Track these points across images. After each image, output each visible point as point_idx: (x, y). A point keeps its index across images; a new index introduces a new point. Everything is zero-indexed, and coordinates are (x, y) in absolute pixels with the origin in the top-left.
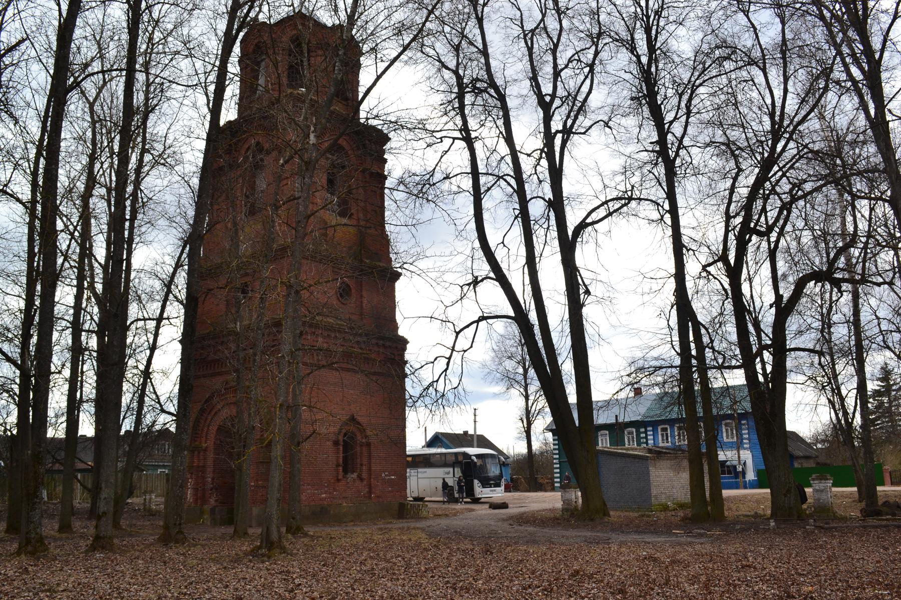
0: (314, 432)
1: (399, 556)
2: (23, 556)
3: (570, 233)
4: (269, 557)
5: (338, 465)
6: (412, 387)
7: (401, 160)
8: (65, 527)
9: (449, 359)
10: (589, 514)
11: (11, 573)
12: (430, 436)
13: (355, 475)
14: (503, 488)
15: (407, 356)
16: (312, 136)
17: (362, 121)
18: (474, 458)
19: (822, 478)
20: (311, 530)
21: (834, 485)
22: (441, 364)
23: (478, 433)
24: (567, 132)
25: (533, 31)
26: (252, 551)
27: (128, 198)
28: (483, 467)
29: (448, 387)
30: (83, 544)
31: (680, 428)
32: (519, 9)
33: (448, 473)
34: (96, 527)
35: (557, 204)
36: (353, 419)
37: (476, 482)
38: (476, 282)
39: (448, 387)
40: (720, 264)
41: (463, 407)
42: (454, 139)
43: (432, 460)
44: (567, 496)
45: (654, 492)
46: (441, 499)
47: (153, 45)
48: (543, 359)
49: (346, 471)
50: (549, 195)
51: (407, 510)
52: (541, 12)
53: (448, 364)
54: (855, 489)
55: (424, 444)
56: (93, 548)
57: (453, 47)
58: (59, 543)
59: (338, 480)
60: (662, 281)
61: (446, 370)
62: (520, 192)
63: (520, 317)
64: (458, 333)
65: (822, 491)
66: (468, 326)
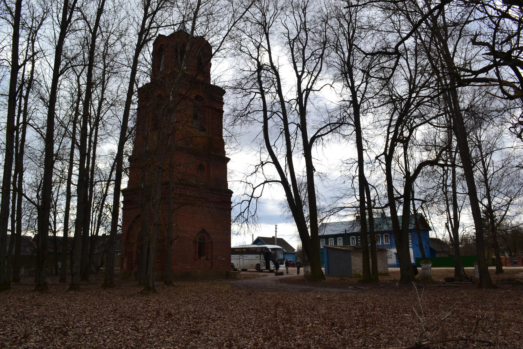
0: (178, 236)
3: (309, 140)
4: (147, 294)
5: (196, 253)
6: (234, 214)
7: (231, 102)
8: (63, 280)
9: (250, 201)
10: (314, 278)
11: (27, 298)
12: (255, 239)
13: (204, 258)
14: (285, 265)
15: (232, 199)
17: (212, 83)
18: (270, 250)
19: (426, 262)
20: (175, 283)
21: (433, 266)
22: (245, 205)
23: (277, 237)
24: (308, 90)
25: (294, 40)
26: (141, 291)
28: (275, 255)
29: (250, 215)
30: (67, 287)
31: (386, 236)
32: (287, 29)
33: (258, 257)
34: (72, 279)
35: (303, 126)
37: (271, 262)
38: (262, 164)
39: (250, 215)
40: (383, 156)
41: (259, 225)
42: (256, 93)
43: (258, 250)
45: (353, 268)
46: (255, 270)
47: (107, 47)
48: (301, 202)
49: (200, 256)
50: (299, 121)
51: (230, 273)
52: (298, 30)
53: (249, 204)
54: (454, 268)
55: (252, 242)
56: (70, 289)
59: (196, 260)
60: (351, 165)
61: (248, 207)
62: (285, 120)
63: (284, 182)
64: (254, 189)
65: (426, 269)
66: (259, 186)
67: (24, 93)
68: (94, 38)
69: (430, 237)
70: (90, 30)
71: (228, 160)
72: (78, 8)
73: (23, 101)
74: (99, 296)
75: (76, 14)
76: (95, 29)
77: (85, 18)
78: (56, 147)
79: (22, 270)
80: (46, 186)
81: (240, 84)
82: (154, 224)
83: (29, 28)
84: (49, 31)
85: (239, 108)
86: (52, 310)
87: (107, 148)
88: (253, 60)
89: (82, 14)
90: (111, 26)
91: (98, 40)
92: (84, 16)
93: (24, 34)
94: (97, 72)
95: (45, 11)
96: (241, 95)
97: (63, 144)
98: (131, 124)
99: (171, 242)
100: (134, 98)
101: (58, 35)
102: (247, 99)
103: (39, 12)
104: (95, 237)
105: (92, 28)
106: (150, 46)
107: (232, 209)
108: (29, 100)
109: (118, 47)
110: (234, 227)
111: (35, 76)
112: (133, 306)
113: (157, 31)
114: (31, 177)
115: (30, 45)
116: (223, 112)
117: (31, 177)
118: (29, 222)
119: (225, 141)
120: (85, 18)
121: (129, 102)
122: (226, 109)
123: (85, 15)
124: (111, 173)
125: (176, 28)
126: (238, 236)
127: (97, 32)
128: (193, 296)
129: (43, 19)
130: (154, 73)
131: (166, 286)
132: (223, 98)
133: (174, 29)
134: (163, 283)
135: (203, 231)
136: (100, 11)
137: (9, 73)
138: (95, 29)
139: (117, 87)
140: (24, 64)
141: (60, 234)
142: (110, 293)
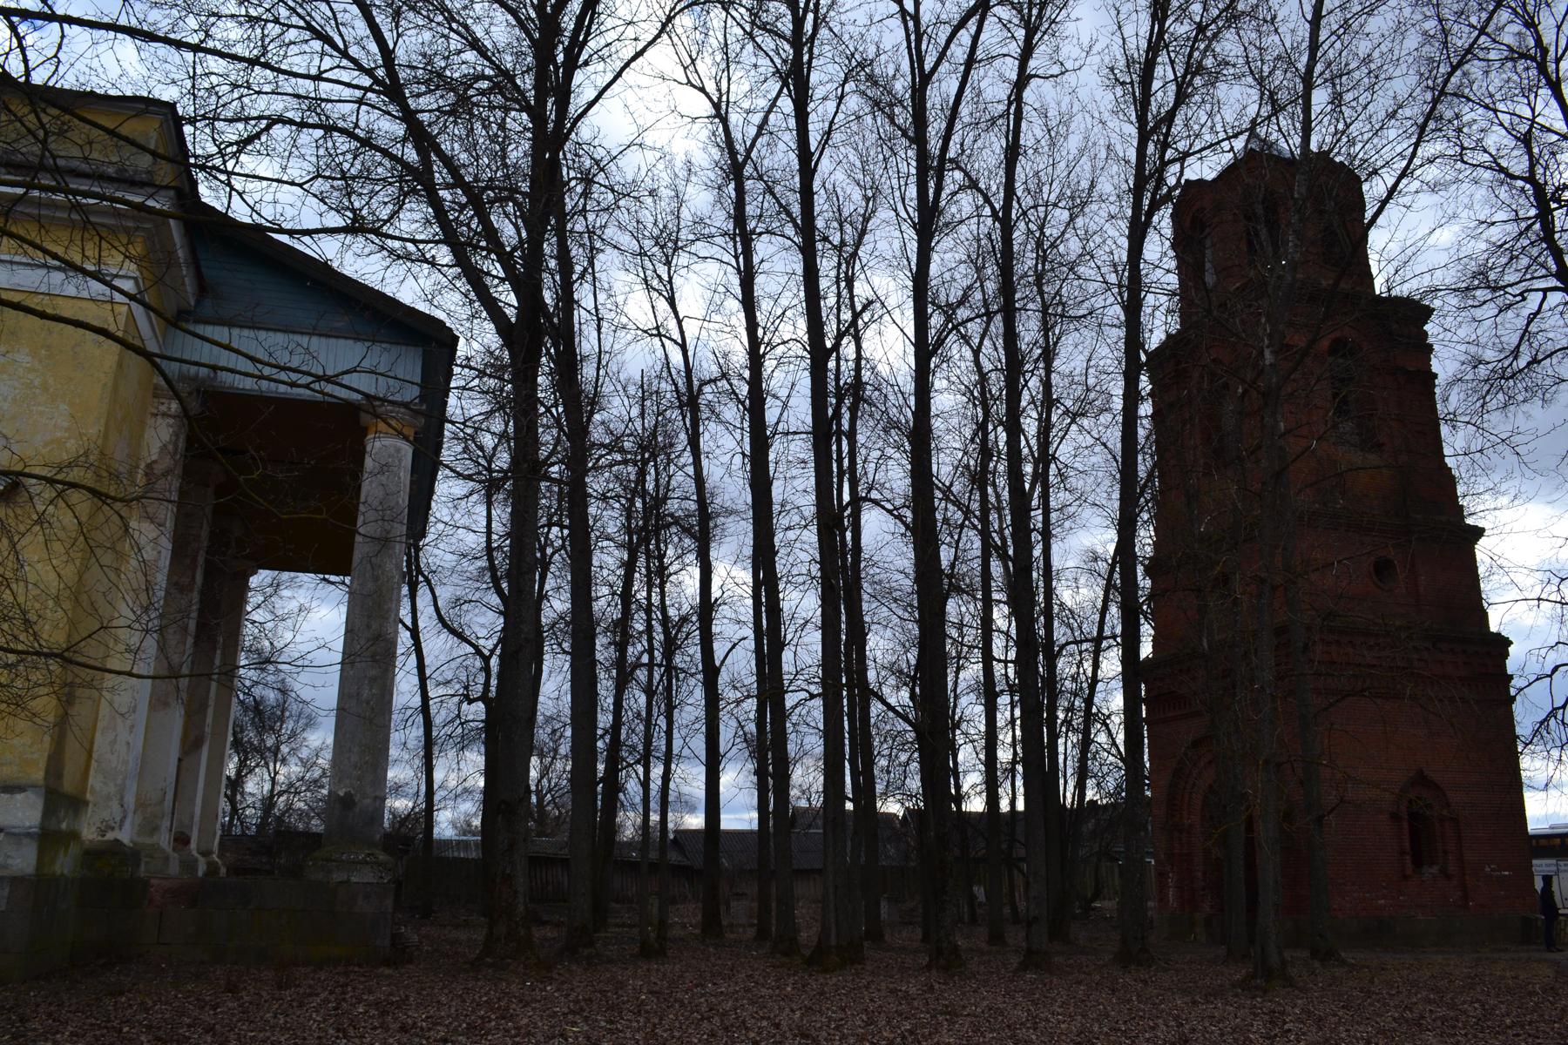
1: (1478, 1001)
2: (934, 972)
4: (1265, 992)
6: (1525, 718)
7: (1450, 350)
8: (996, 938)
11: (913, 990)
13: (1435, 869)
15: (1511, 665)
16: (1267, 354)
27: (602, 737)
30: (1015, 961)
36: (1421, 779)
42: (1545, 291)
44: (74, 850)
49: (1418, 863)
56: (1024, 966)
57: (1518, 139)
58: (985, 958)
67: (846, 425)
68: (1007, 228)
69: (755, 826)
70: (994, 213)
71: (1478, 532)
72: (951, 161)
73: (845, 443)
74: (1113, 991)
75: (954, 178)
76: (1007, 207)
77: (973, 184)
78: (946, 555)
79: (884, 908)
80: (930, 674)
81: (1482, 273)
82: (1266, 762)
83: (835, 247)
84: (890, 238)
85: (1490, 355)
86: (992, 1031)
87: (1083, 542)
88: (1520, 183)
89: (967, 174)
90: (1046, 189)
91: (1018, 235)
92: (970, 178)
93: (827, 265)
94: (1029, 329)
95: (870, 193)
96: (1490, 310)
97: (961, 550)
98: (1143, 466)
99: (1320, 819)
100: (1145, 383)
101: (913, 246)
102: (1514, 322)
103: (854, 199)
104: (1086, 810)
105: (997, 206)
106: (1164, 220)
107: (1513, 699)
108: (861, 439)
109: (1073, 246)
110: (1532, 766)
111: (866, 375)
112: (1234, 1031)
113: (1182, 169)
114: (887, 644)
115: (845, 293)
116: (1435, 376)
117: (887, 644)
118: (888, 772)
119: (1455, 472)
120: (973, 184)
121: (1132, 397)
122: (1444, 365)
123: (973, 174)
124: (1104, 611)
125: (1239, 144)
126: (1553, 792)
127: (1014, 212)
128: (1430, 1002)
129: (866, 220)
130: (1189, 296)
131: (1317, 964)
132: (1426, 333)
133: (1232, 149)
134: (1306, 953)
135: (1420, 778)
136: (1013, 153)
137: (807, 373)
138: (1007, 207)
139: (1089, 357)
140: (836, 347)
141: (976, 805)
142: (1145, 982)
